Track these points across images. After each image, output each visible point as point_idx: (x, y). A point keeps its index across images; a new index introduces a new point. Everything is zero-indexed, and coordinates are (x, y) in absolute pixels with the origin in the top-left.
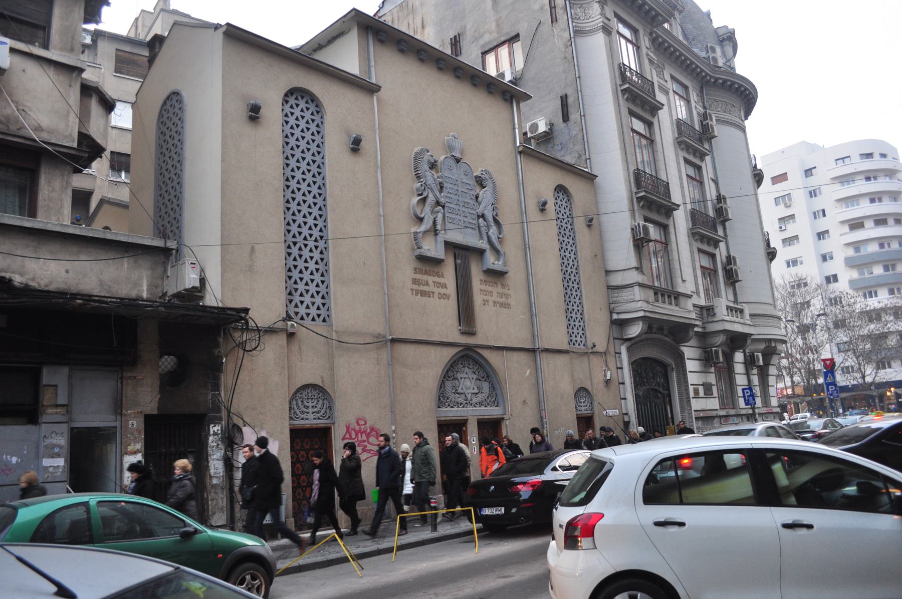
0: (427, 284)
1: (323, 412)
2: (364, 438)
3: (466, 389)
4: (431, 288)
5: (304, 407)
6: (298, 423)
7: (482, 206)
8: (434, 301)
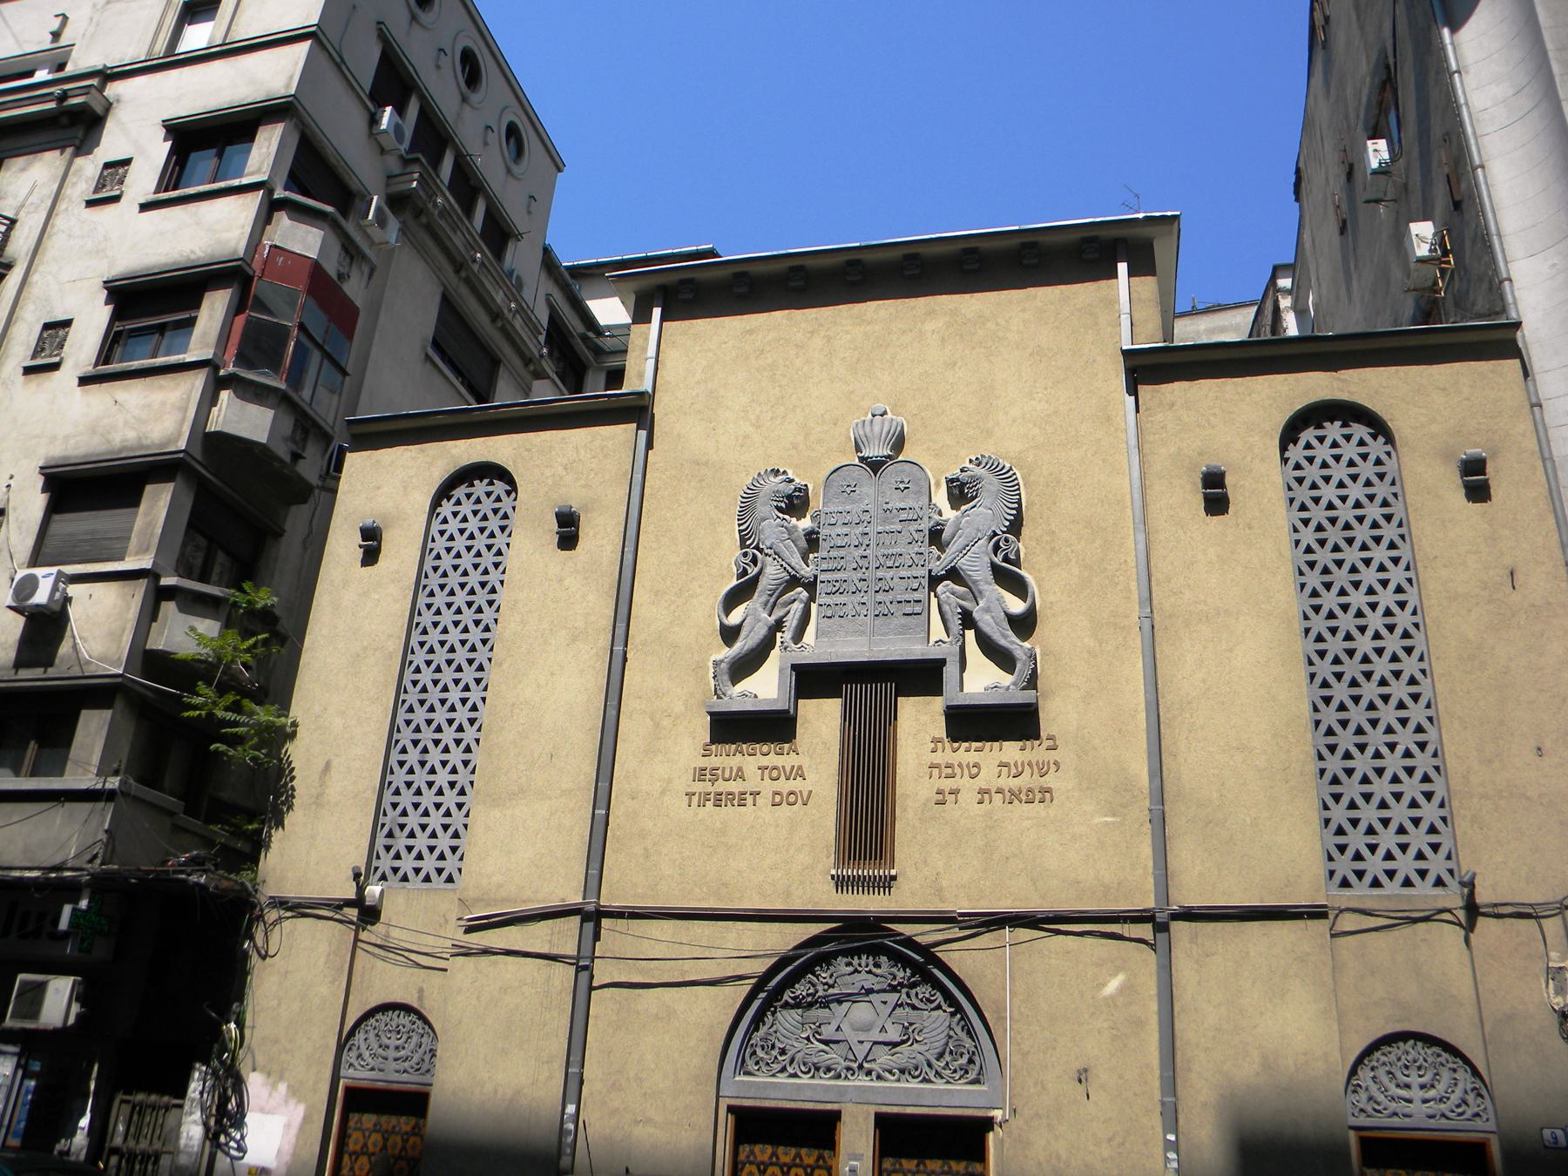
1: (416, 1058)
4: (753, 781)
5: (1398, 1086)
7: (952, 550)
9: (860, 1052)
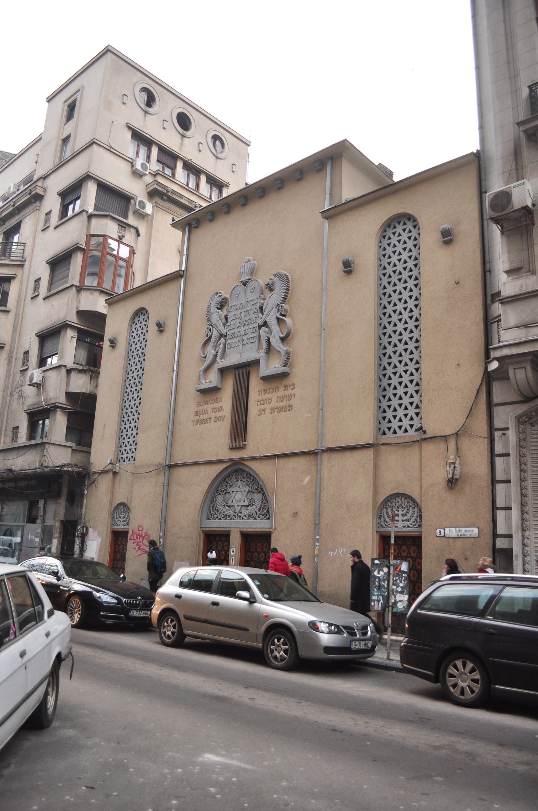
0: (206, 412)
2: (141, 540)
3: (237, 502)
6: (116, 527)
8: (211, 425)
9: (237, 510)
